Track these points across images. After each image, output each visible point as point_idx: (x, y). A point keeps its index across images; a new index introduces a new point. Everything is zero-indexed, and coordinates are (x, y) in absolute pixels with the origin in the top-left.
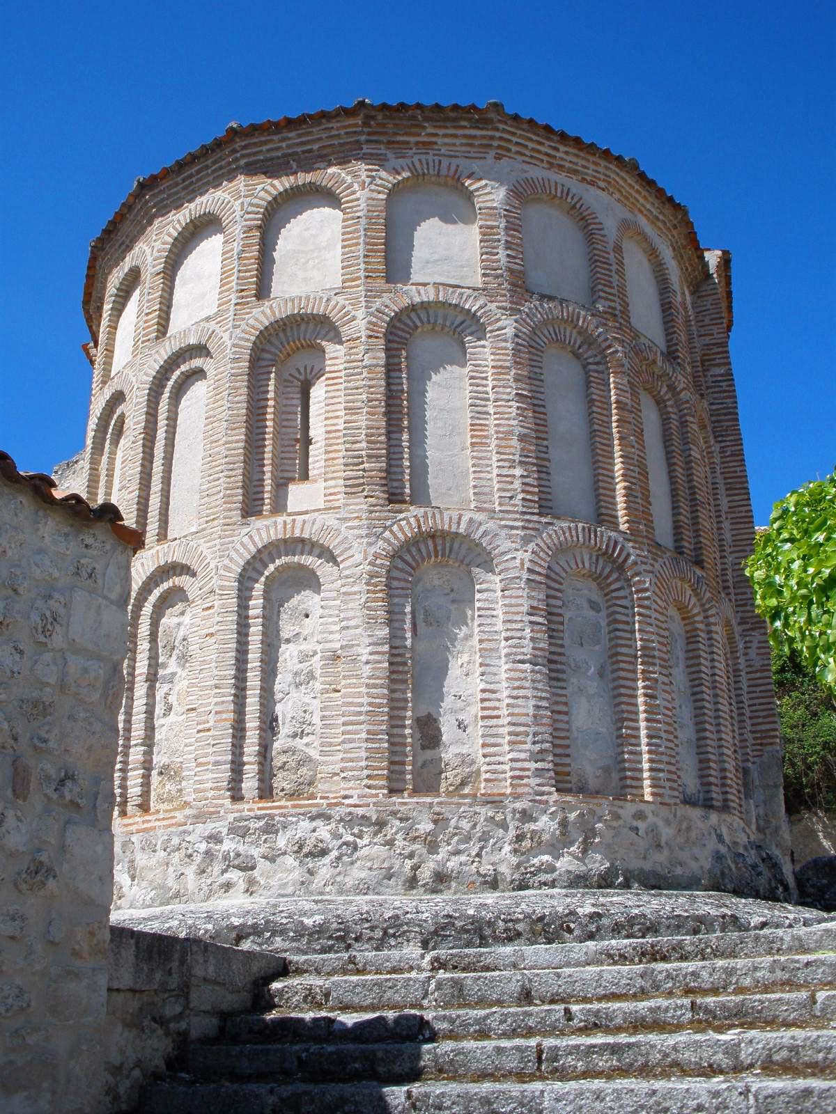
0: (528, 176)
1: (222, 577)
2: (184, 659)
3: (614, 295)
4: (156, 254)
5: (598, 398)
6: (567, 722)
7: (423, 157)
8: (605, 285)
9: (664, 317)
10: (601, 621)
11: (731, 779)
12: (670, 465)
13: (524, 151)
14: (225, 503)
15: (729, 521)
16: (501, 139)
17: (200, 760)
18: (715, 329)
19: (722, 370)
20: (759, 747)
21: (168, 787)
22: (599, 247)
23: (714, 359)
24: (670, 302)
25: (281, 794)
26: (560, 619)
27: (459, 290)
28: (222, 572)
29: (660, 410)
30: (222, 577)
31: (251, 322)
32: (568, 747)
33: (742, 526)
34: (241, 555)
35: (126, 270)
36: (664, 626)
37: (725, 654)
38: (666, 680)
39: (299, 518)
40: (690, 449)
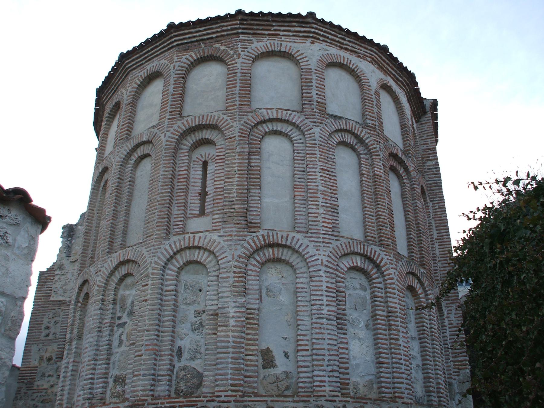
0: (329, 52)
1: (154, 268)
2: (131, 313)
3: (375, 118)
4: (128, 93)
5: (366, 173)
6: (347, 354)
7: (272, 42)
8: (370, 112)
9: (402, 132)
10: (367, 296)
11: (443, 389)
12: (405, 211)
13: (326, 40)
14: (157, 226)
15: (438, 244)
16: (314, 33)
17: (136, 373)
18: (429, 141)
19: (433, 163)
20: (457, 370)
21: (118, 389)
22: (367, 92)
23: (429, 157)
24: (406, 124)
25: (181, 394)
26: (344, 295)
27: (289, 112)
28: (153, 265)
29: (400, 182)
30: (154, 268)
31: (176, 128)
32: (348, 368)
33: (445, 246)
34: (164, 256)
35: (114, 103)
36: (403, 299)
37: (437, 317)
38: (404, 331)
39: (197, 235)
40: (416, 203)
